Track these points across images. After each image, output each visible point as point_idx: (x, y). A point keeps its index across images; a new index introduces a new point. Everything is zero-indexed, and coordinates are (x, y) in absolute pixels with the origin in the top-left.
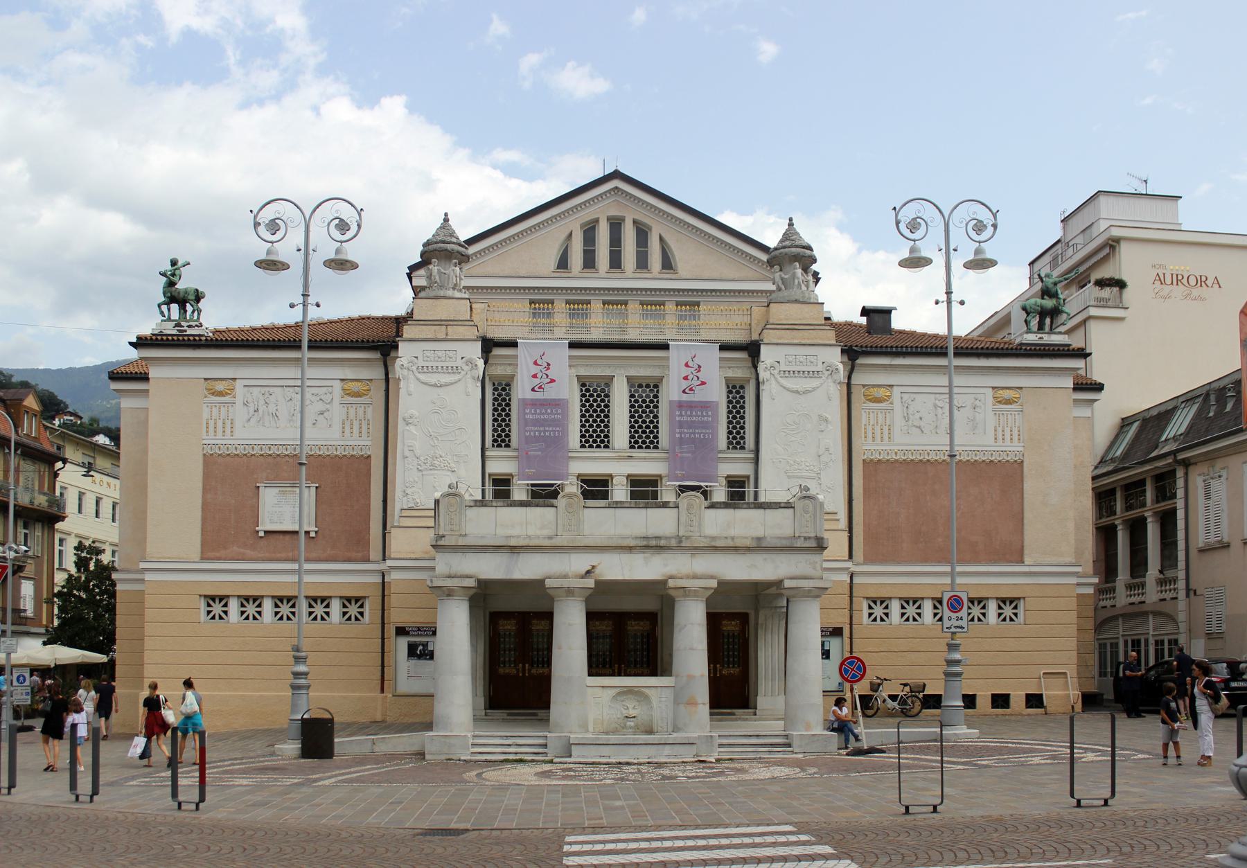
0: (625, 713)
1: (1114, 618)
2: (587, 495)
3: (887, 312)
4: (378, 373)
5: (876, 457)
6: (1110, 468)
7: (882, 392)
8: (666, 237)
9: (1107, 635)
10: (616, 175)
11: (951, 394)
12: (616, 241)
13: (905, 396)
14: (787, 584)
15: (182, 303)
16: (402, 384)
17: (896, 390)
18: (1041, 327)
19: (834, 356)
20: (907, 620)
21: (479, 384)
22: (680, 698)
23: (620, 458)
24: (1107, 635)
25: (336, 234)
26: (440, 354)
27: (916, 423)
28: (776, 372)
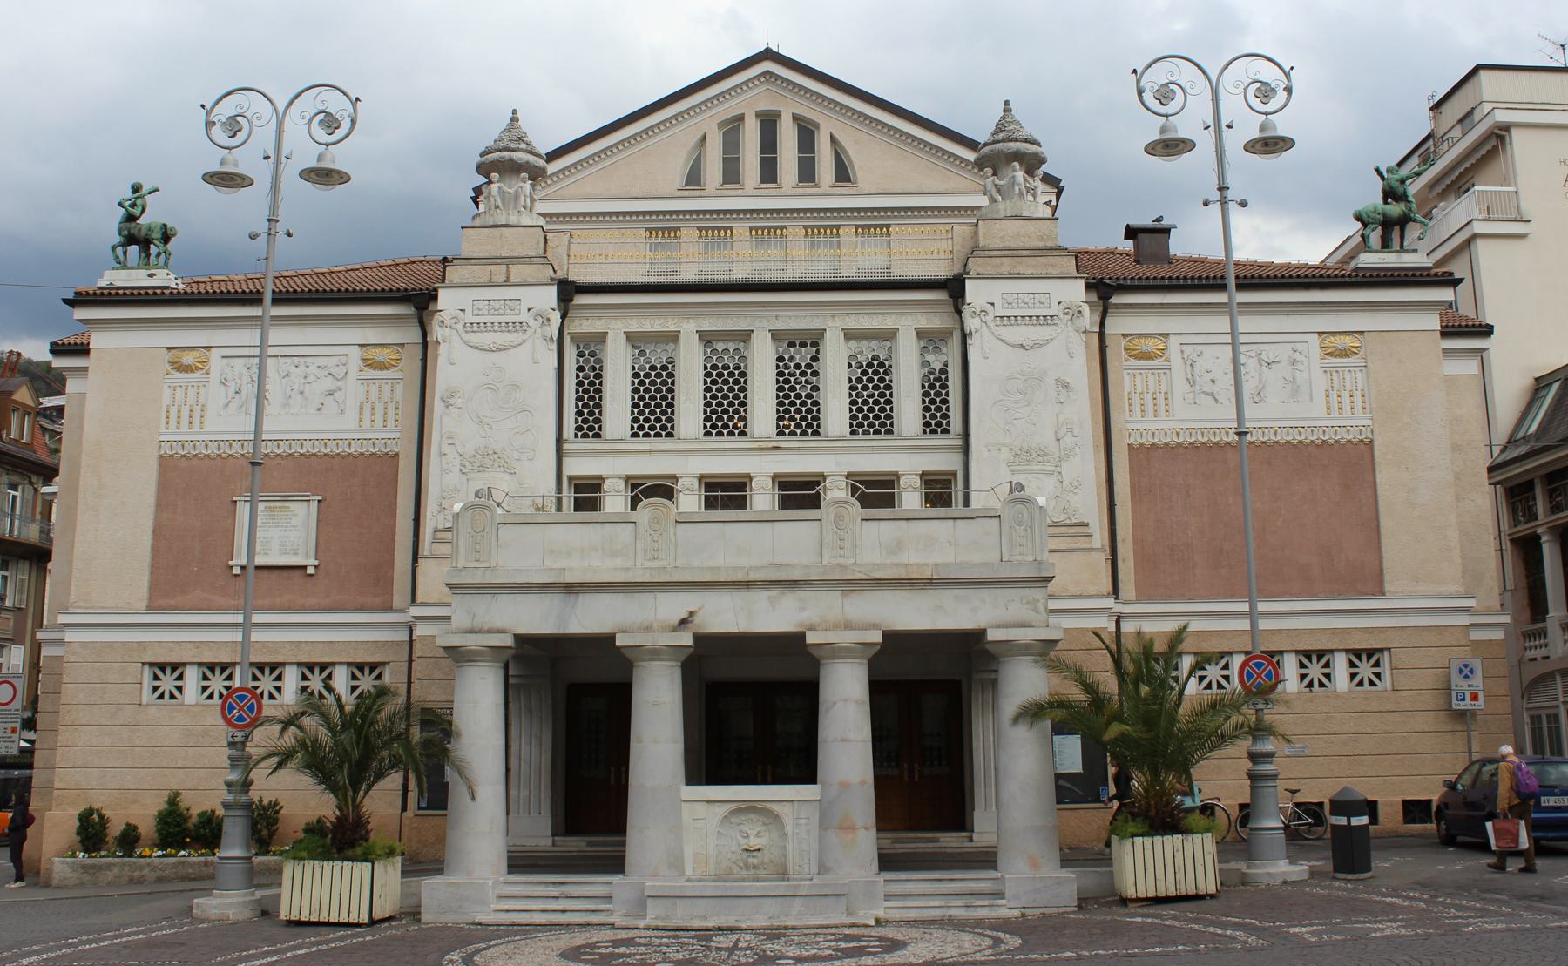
0: (744, 843)
1: (1547, 677)
2: (786, 503)
3: (1161, 232)
4: (414, 335)
5: (1148, 439)
6: (1523, 450)
7: (1151, 345)
8: (839, 137)
9: (1540, 702)
10: (768, 55)
11: (1234, 344)
12: (769, 143)
13: (1188, 349)
14: (992, 635)
15: (144, 243)
16: (442, 349)
17: (215, 355)
18: (1386, 245)
19: (1076, 291)
20: (161, 697)
21: (554, 346)
22: (827, 818)
23: (761, 449)
24: (1540, 702)
25: (321, 135)
26: (496, 304)
27: (1208, 388)
28: (989, 319)
